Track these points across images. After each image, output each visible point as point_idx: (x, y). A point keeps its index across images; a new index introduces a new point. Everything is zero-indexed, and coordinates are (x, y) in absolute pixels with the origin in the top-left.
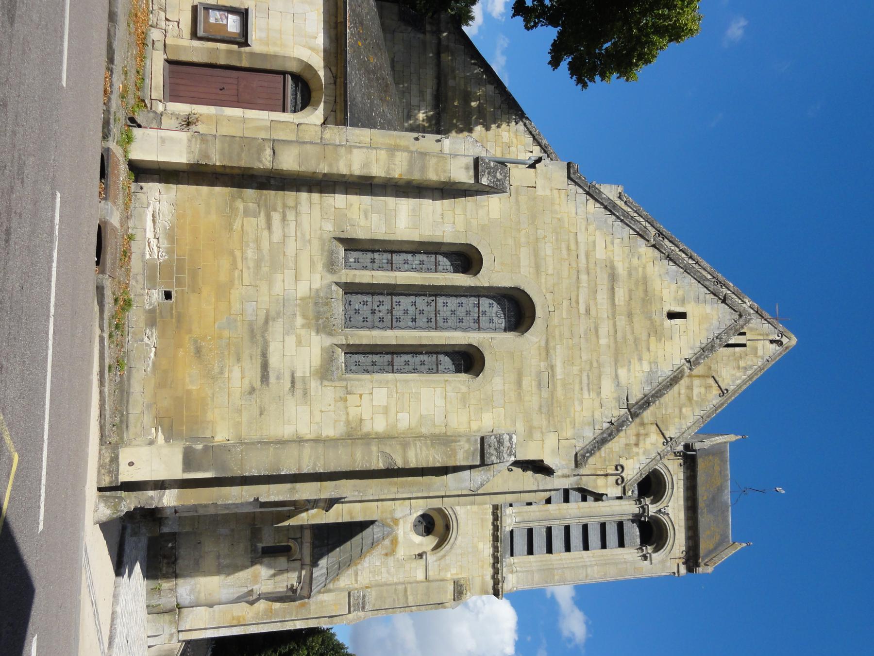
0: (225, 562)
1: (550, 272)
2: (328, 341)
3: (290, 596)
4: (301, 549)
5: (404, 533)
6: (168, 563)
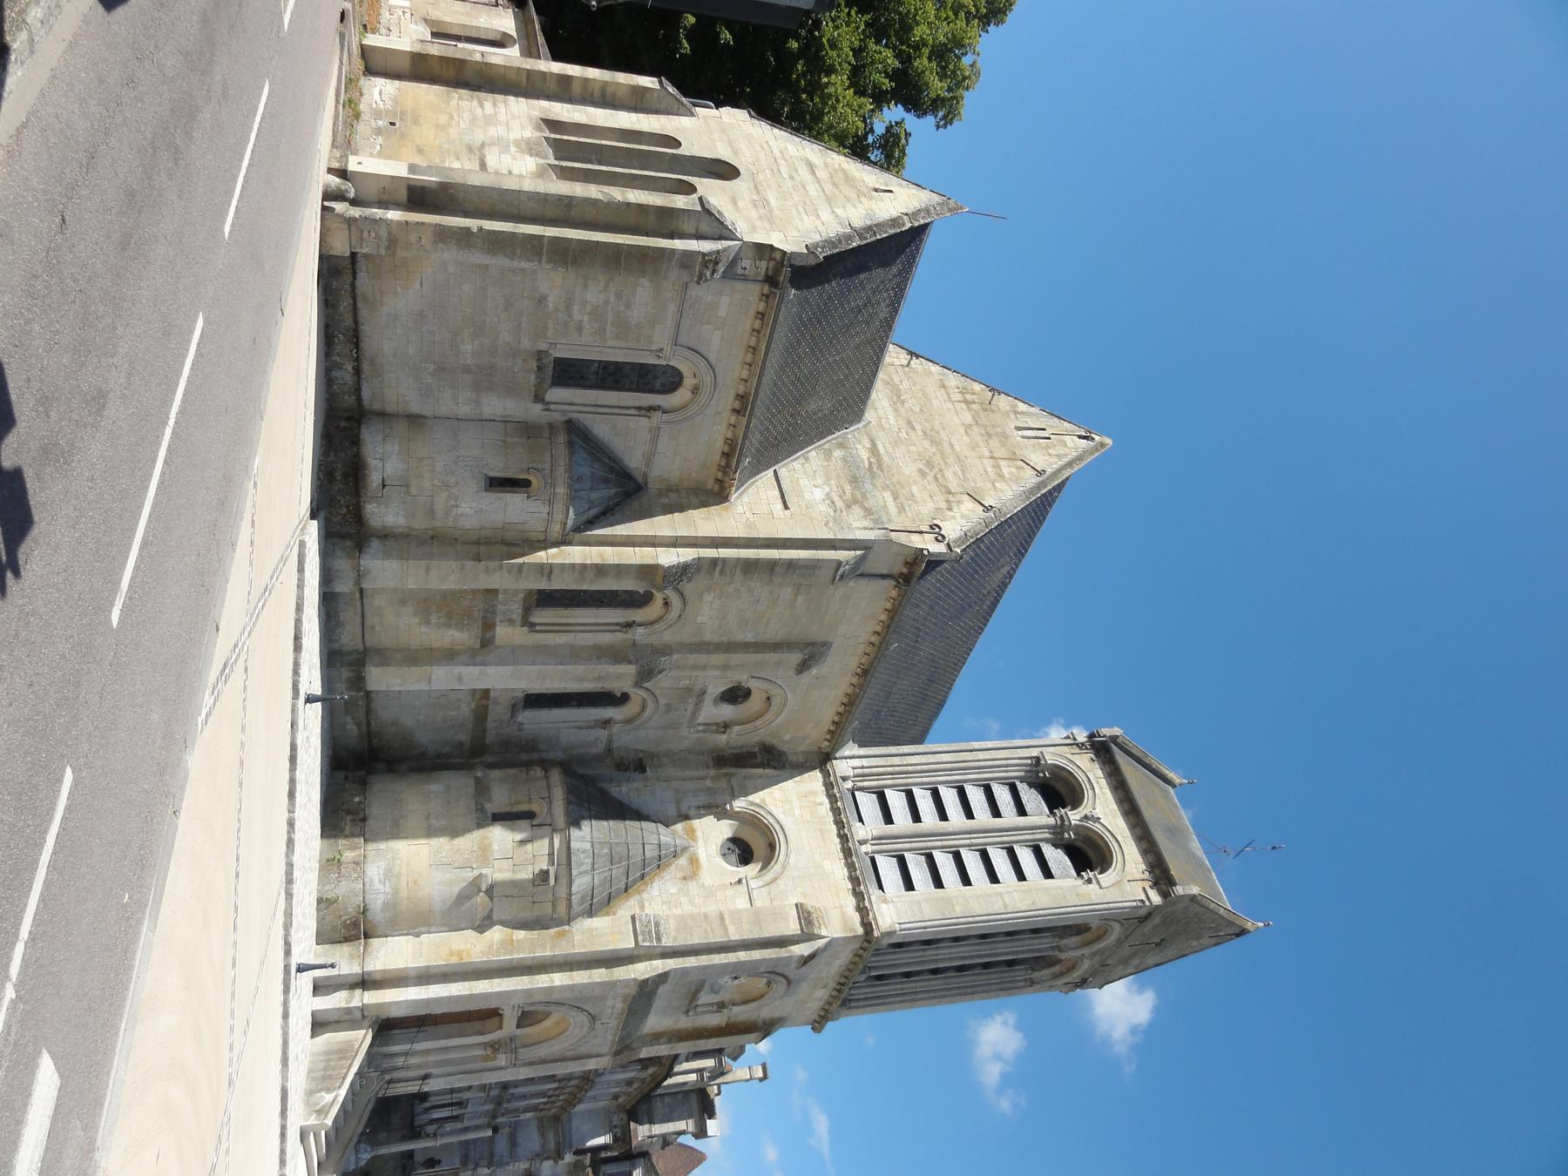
2: (542, 161)
3: (539, 903)
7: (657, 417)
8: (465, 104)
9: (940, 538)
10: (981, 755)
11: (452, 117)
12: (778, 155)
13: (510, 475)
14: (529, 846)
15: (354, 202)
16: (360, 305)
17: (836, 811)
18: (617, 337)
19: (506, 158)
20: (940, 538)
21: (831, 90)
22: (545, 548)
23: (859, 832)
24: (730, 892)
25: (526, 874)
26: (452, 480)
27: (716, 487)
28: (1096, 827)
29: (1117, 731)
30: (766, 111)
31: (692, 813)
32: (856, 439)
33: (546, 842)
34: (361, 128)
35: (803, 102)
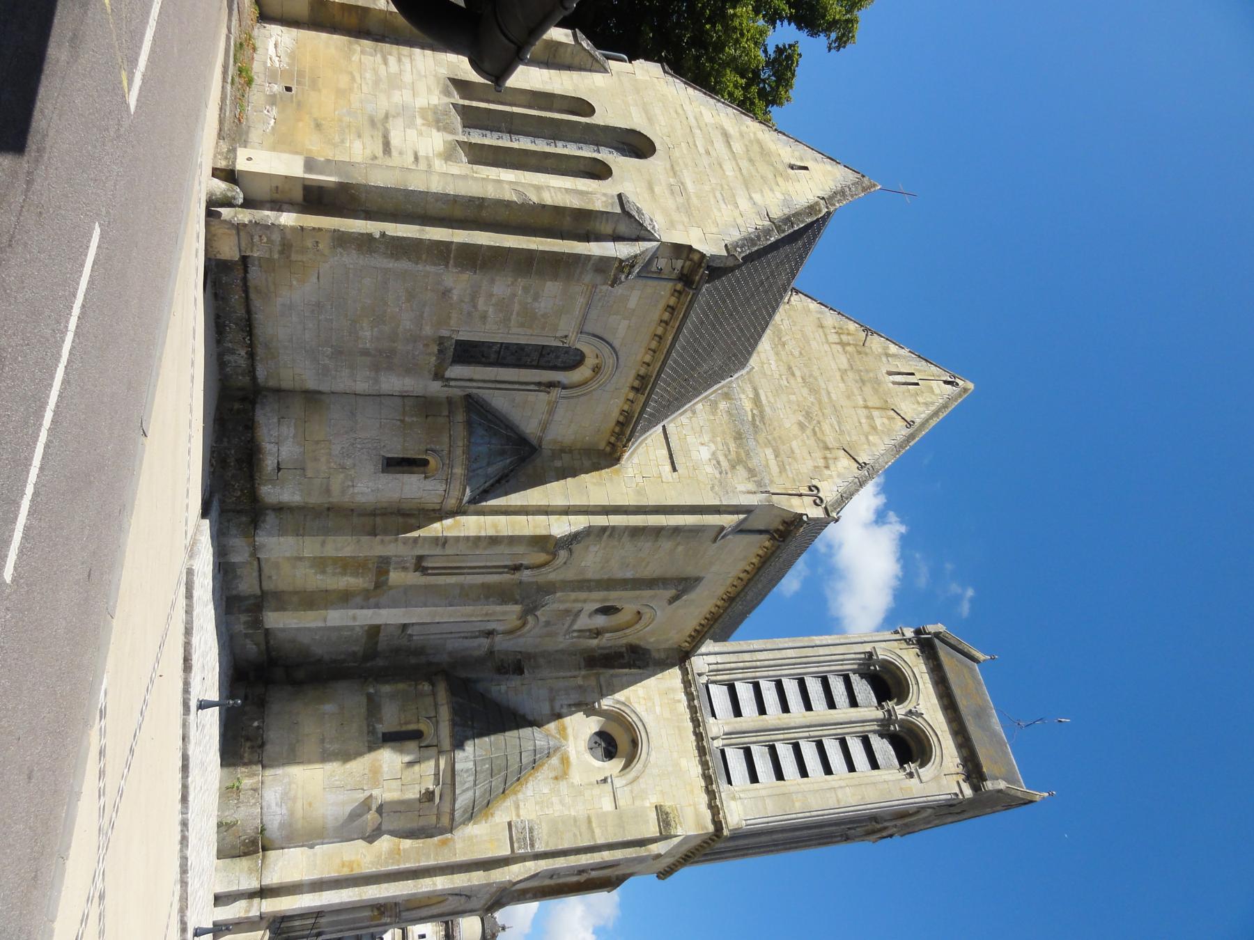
0: (335, 747)
1: (663, 123)
2: (450, 137)
3: (426, 818)
4: (436, 730)
5: (577, 752)
6: (252, 747)
7: (555, 392)
8: (367, 59)
9: (818, 502)
10: (821, 651)
11: (353, 79)
12: (693, 122)
13: (410, 455)
14: (417, 768)
15: (249, 204)
16: (253, 295)
17: (693, 710)
18: (522, 325)
19: (412, 134)
20: (818, 502)
21: (736, 23)
22: (440, 519)
23: (714, 727)
24: (597, 790)
25: (413, 794)
26: (349, 462)
27: (608, 449)
28: (919, 721)
29: (940, 628)
30: (678, 67)
31: (564, 710)
32: (738, 383)
33: (432, 763)
34: (256, 96)
35: (707, 32)
